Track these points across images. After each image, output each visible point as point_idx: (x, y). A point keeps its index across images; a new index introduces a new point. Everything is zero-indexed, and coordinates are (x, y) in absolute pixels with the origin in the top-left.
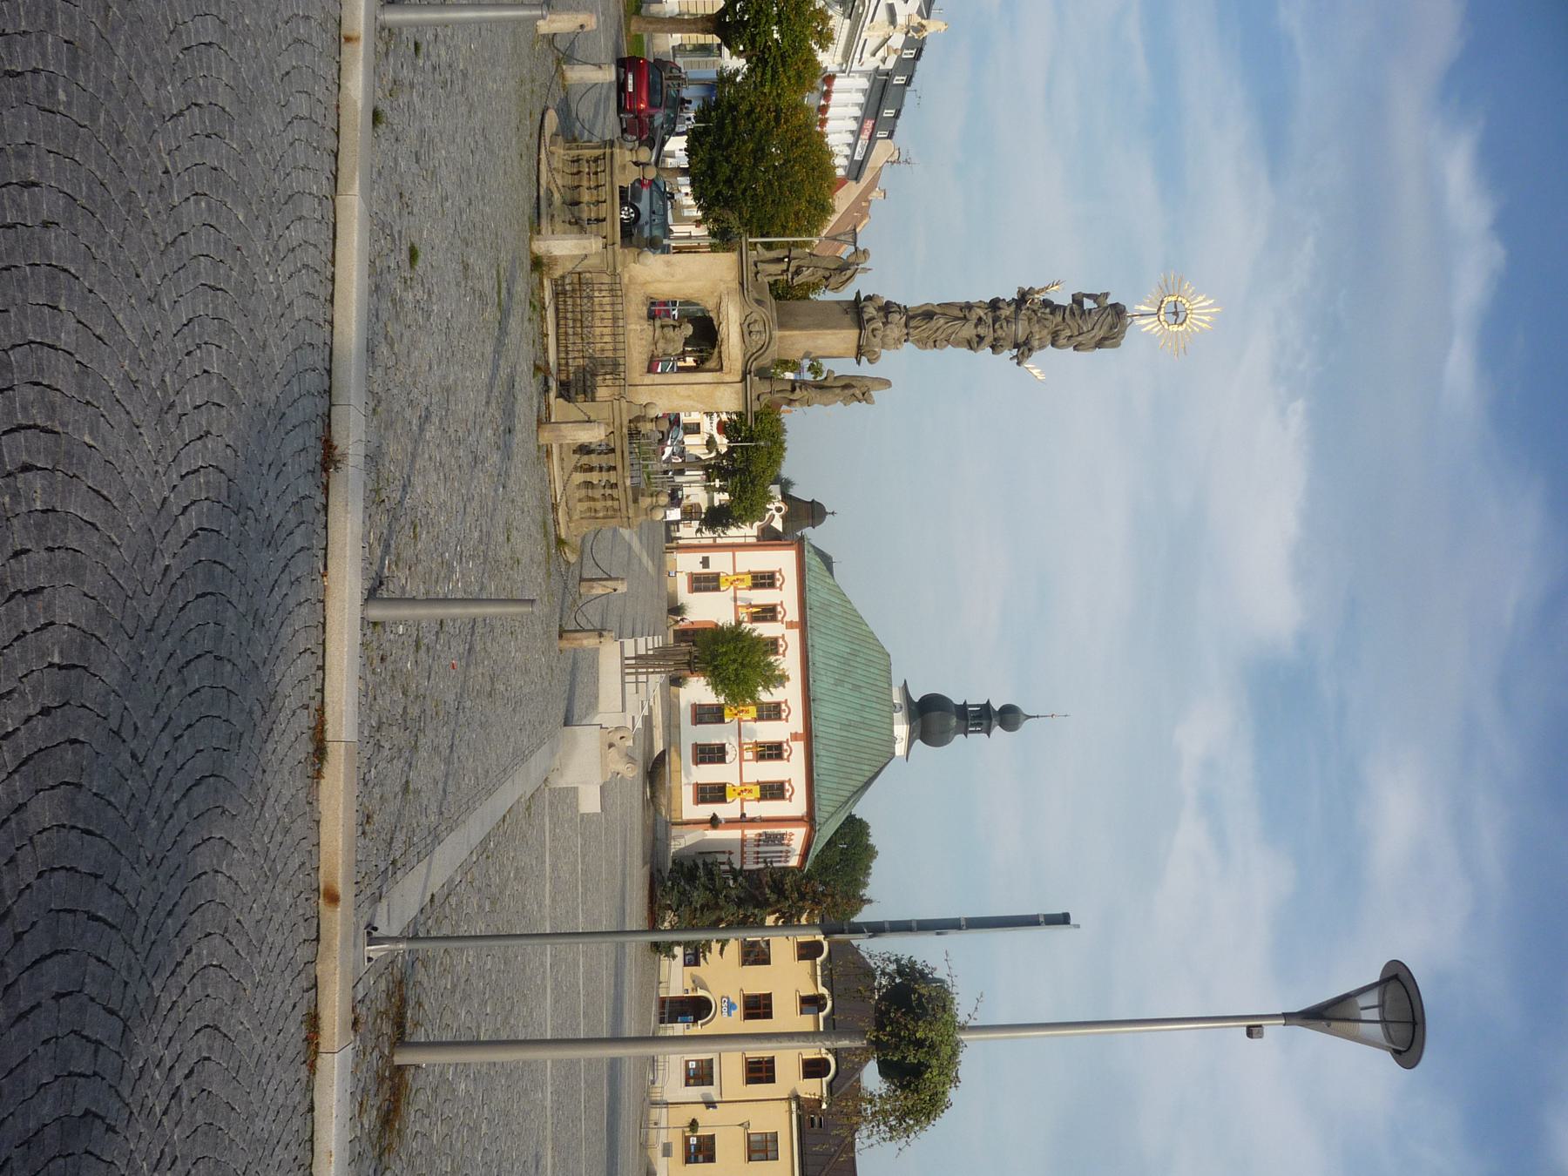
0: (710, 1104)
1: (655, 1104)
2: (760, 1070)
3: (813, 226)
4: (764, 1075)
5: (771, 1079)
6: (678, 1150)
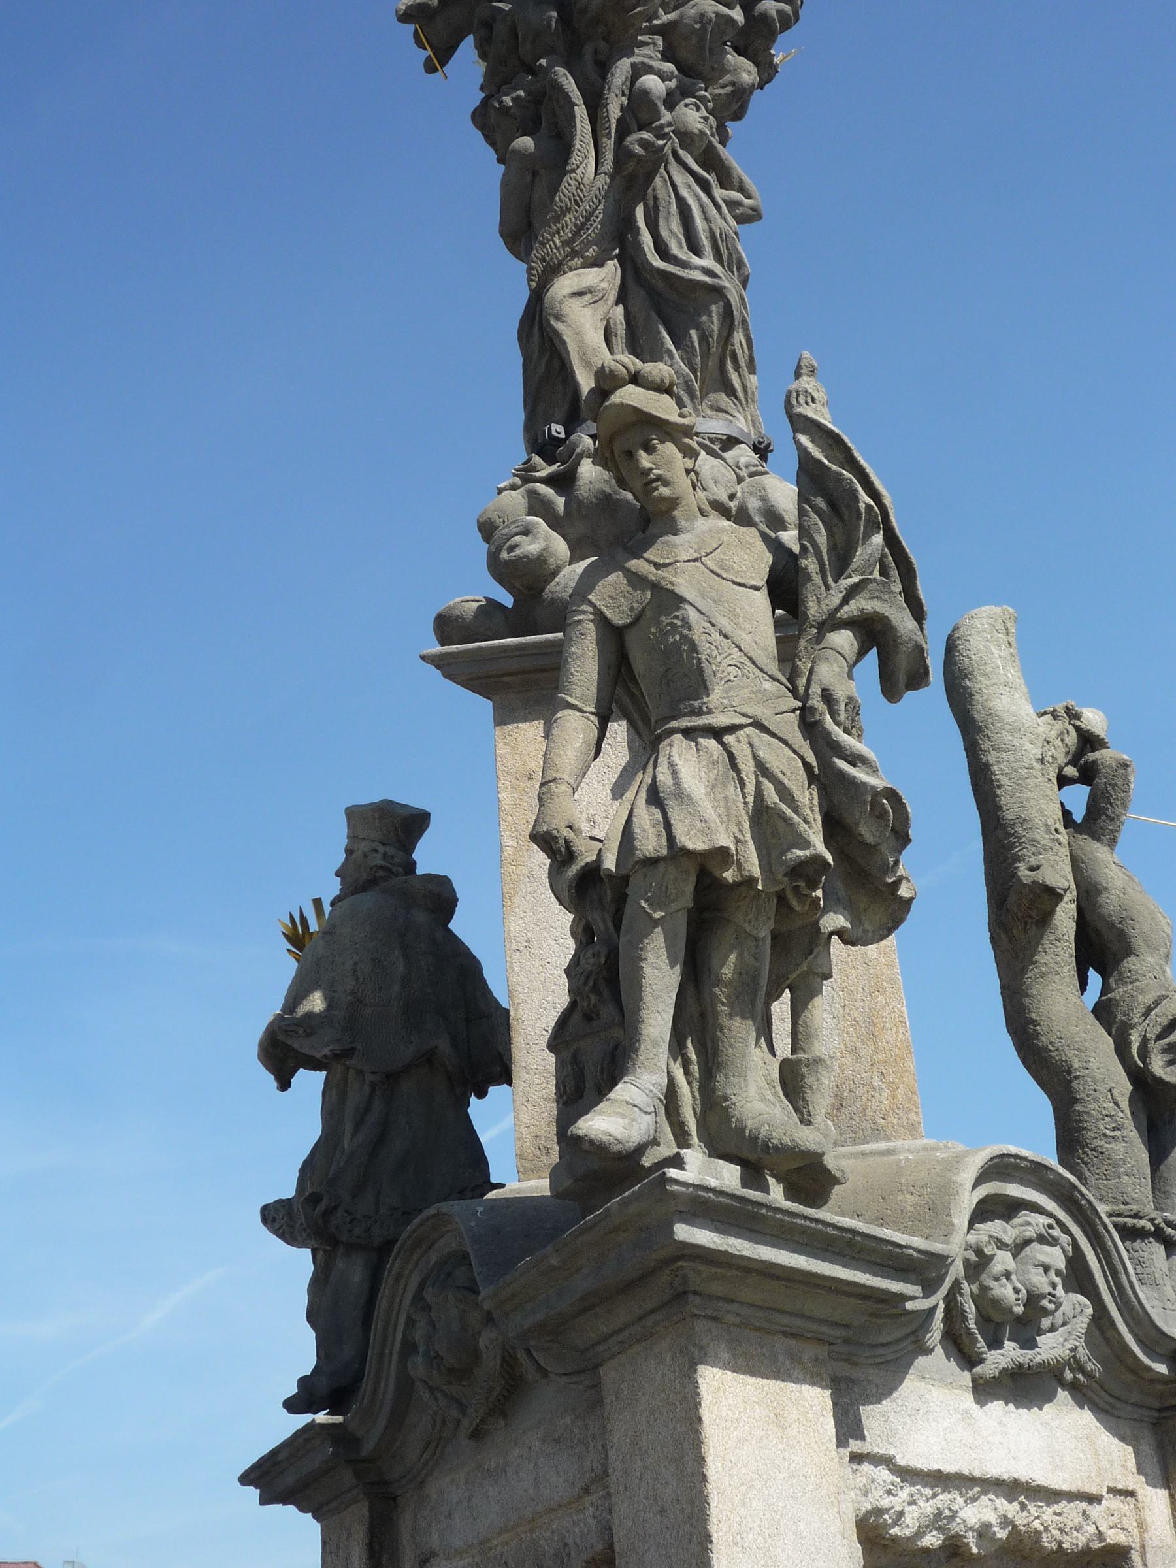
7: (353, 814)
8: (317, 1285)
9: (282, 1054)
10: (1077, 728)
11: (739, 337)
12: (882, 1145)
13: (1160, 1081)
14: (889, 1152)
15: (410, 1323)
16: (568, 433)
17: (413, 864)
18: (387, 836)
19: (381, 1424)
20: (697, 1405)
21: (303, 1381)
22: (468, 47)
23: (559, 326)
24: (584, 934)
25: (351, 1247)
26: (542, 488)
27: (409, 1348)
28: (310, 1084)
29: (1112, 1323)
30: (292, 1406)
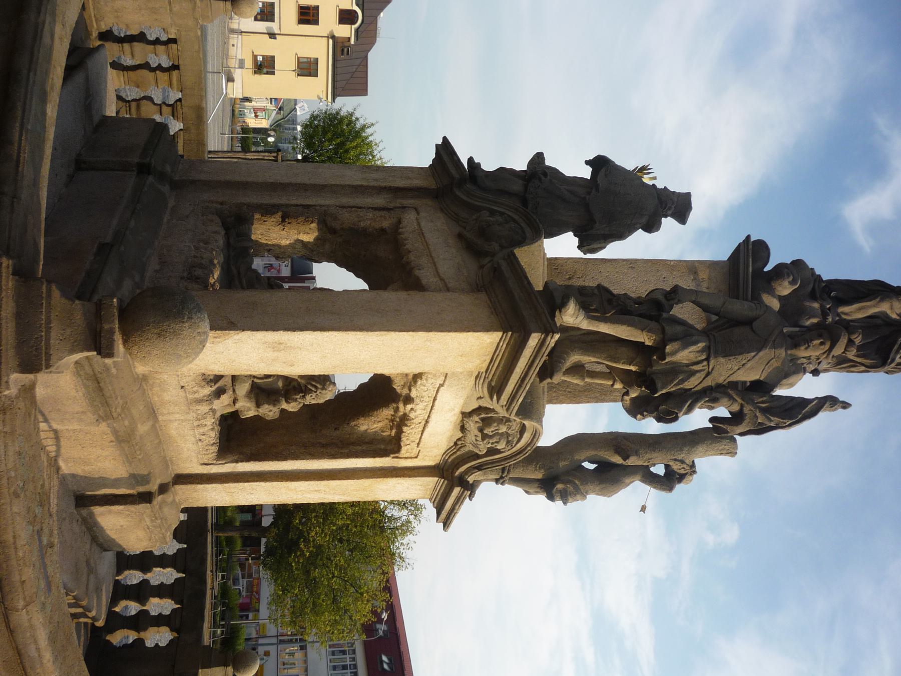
0: (272, 35)
1: (233, 31)
2: (307, 14)
3: (777, 368)
4: (311, 18)
5: (316, 22)
6: (249, 63)
7: (688, 196)
8: (512, 172)
9: (599, 164)
10: (686, 474)
11: (863, 368)
12: (546, 390)
13: (554, 486)
15: (502, 214)
17: (666, 217)
18: (679, 206)
19: (465, 198)
20: (474, 331)
21: (479, 164)
23: (878, 300)
24: (638, 301)
25: (526, 187)
26: (811, 286)
27: (492, 213)
28: (586, 173)
29: (475, 460)
30: (471, 160)
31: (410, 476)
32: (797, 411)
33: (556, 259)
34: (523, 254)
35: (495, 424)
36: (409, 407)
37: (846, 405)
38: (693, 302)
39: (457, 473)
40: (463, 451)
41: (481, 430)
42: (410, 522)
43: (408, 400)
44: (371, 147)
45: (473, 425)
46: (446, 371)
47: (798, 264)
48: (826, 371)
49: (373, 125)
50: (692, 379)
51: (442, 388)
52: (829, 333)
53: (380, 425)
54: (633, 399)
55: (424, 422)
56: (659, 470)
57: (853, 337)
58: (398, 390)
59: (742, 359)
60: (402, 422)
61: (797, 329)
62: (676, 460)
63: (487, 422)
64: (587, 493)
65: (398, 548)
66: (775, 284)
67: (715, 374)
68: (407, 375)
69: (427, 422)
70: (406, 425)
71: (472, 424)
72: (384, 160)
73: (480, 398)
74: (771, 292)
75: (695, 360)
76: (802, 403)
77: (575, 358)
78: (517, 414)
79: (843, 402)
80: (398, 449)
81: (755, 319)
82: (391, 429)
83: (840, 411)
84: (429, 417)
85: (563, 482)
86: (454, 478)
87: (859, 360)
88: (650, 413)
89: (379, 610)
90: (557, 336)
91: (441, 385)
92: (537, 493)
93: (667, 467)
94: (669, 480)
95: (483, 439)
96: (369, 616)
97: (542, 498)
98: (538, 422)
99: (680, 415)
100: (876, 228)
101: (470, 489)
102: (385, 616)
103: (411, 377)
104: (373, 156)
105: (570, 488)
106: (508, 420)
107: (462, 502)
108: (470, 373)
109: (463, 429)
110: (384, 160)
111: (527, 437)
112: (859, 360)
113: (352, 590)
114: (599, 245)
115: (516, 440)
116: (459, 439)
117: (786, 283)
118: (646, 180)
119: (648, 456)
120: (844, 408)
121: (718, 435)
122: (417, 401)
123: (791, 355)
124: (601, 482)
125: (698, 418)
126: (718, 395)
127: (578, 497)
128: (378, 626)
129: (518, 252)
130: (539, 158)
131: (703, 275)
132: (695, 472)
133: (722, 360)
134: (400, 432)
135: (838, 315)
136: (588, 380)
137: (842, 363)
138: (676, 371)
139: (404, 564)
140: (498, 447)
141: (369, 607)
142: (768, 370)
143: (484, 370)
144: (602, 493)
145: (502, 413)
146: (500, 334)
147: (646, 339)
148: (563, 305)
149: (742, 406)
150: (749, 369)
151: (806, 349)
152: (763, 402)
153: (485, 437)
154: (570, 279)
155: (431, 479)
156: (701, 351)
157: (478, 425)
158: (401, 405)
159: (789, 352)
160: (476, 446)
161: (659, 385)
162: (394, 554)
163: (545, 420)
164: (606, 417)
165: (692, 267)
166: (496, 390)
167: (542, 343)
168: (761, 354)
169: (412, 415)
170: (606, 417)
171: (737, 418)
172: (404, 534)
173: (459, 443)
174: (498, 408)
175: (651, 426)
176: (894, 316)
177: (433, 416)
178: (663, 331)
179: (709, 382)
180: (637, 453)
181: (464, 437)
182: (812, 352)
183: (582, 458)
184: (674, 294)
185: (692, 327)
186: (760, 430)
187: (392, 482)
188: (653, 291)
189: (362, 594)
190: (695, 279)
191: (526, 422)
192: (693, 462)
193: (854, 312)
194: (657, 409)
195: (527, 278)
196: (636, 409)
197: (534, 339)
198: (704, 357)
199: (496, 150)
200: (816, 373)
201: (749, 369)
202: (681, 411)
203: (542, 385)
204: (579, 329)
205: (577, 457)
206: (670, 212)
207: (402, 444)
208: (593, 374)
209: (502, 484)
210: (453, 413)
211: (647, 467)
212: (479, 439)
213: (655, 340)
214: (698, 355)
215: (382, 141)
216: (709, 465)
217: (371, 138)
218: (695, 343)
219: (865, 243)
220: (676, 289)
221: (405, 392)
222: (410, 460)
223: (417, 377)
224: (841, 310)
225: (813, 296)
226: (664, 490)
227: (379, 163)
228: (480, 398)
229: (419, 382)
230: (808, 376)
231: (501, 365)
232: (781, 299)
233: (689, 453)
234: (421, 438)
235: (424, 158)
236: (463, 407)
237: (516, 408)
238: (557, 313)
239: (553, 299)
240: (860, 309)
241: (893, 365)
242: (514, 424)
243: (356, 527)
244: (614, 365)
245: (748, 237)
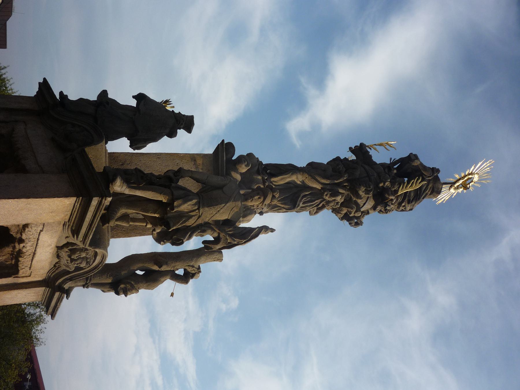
7: (192, 117)
8: (87, 101)
9: (140, 98)
11: (285, 210)
12: (110, 230)
14: (108, 231)
16: (268, 174)
17: (180, 129)
18: (187, 123)
21: (67, 96)
22: (354, 157)
24: (159, 177)
26: (257, 167)
28: (133, 103)
30: (61, 93)
31: (26, 288)
32: (249, 235)
33: (114, 153)
34: (91, 152)
35: (78, 253)
36: (22, 245)
37: (273, 230)
38: (190, 177)
39: (57, 284)
40: (59, 270)
41: (69, 256)
42: (42, 316)
43: (21, 241)
44: (4, 82)
45: (64, 254)
46: (43, 222)
47: (250, 155)
48: (267, 212)
49: (5, 67)
50: (190, 220)
51: (42, 233)
52: (263, 193)
53: (4, 258)
54: (158, 233)
55: (32, 254)
56: (180, 272)
57: (275, 194)
58: (14, 235)
59: (218, 208)
60: (20, 253)
61: (251, 190)
62: (189, 266)
63: (73, 252)
64: (139, 288)
65: (35, 333)
66: (238, 167)
67: (203, 217)
68: (18, 225)
69: (34, 254)
70: (21, 257)
71: (64, 254)
72: (14, 91)
73: (67, 237)
74: (236, 170)
75: (191, 209)
76: (250, 230)
77: (123, 211)
78: (90, 245)
79: (271, 229)
80: (17, 272)
81: (224, 186)
82: (12, 260)
83: (270, 233)
84: (35, 251)
85: (123, 284)
86: (56, 286)
87: (282, 206)
88: (168, 240)
89: (24, 374)
90: (110, 199)
91: (41, 231)
92: (109, 291)
93: (185, 270)
94: (185, 278)
95: (71, 262)
96: (17, 378)
97: (112, 294)
98: (104, 250)
99: (184, 241)
100: (302, 135)
101: (68, 293)
102: (29, 376)
103: (21, 227)
104: (6, 88)
105: (129, 286)
106: (87, 250)
107: (61, 301)
108: (59, 223)
109: (58, 256)
110: (14, 91)
111: (98, 259)
112: (282, 206)
113: (4, 363)
114: (142, 145)
115: (92, 261)
116: (57, 263)
117: (243, 166)
118: (168, 108)
119: (173, 265)
120: (272, 232)
121: (209, 250)
122: (27, 241)
123: (244, 205)
124: (147, 281)
125: (193, 243)
126: (206, 228)
127: (134, 291)
128: (25, 383)
129: (87, 149)
130: (104, 93)
131: (199, 161)
132: (200, 272)
133: (206, 209)
134: (17, 261)
135: (271, 182)
136: (131, 223)
137: (273, 208)
138: (187, 216)
139: (39, 343)
140: (81, 266)
141: (16, 372)
142: (232, 213)
143: (67, 220)
144: (148, 288)
145: (81, 246)
146: (75, 198)
147: (163, 199)
148: (113, 180)
149: (219, 234)
150: (222, 213)
151: (251, 201)
152: (230, 231)
153: (72, 260)
154: (122, 165)
155: (41, 288)
156: (195, 205)
157: (68, 253)
158: (17, 245)
159: (243, 203)
160: (68, 266)
161: (171, 224)
162: (32, 337)
163: (109, 249)
164: (144, 244)
165: (193, 158)
166: (75, 232)
167: (100, 203)
168: (228, 205)
169: (24, 250)
170: (144, 244)
171: (217, 240)
172: (38, 324)
173: (57, 265)
174: (78, 243)
175: (168, 248)
176: (299, 182)
177: (38, 250)
178: (172, 194)
179: (200, 221)
180: (167, 264)
181: (59, 261)
182: (253, 203)
183: (135, 269)
184: (180, 173)
185: (190, 191)
186: (230, 246)
187: (15, 293)
188: (167, 171)
189: (11, 365)
190: (195, 164)
191: (97, 250)
192: (199, 266)
193: (279, 181)
194: (171, 238)
195: (92, 165)
196: (160, 239)
197: (95, 201)
198: (196, 208)
199: (76, 87)
200: (261, 213)
201: (222, 213)
202: (184, 238)
203: (104, 227)
204: (124, 194)
205: (132, 268)
206: (182, 126)
207: (19, 269)
208: (134, 220)
209: (87, 287)
210: (51, 247)
211: (174, 271)
212: (69, 262)
213: (168, 199)
214: (193, 206)
215: (12, 78)
216: (208, 267)
217: (4, 76)
218: (191, 200)
219: (298, 143)
220: (180, 170)
221: (18, 236)
222: (25, 278)
223: (26, 226)
224: (272, 179)
225: (258, 173)
226: (183, 283)
227: (10, 92)
228: (67, 237)
229: (27, 230)
230: (257, 215)
231: (77, 217)
232: (241, 174)
233: (196, 261)
234: (31, 264)
235: (30, 90)
236: (57, 243)
237: (88, 242)
238: (110, 185)
239: (108, 177)
240: (282, 179)
241: (299, 208)
242: (90, 251)
243: (5, 322)
244: (146, 214)
245: (223, 141)
